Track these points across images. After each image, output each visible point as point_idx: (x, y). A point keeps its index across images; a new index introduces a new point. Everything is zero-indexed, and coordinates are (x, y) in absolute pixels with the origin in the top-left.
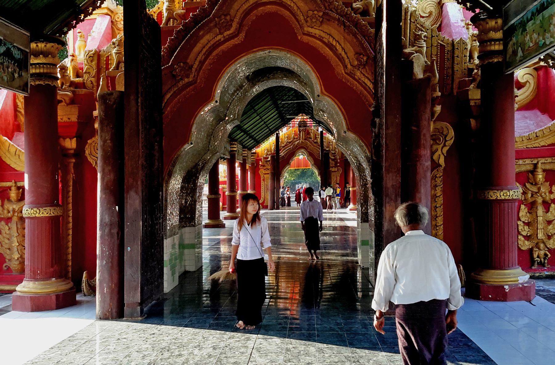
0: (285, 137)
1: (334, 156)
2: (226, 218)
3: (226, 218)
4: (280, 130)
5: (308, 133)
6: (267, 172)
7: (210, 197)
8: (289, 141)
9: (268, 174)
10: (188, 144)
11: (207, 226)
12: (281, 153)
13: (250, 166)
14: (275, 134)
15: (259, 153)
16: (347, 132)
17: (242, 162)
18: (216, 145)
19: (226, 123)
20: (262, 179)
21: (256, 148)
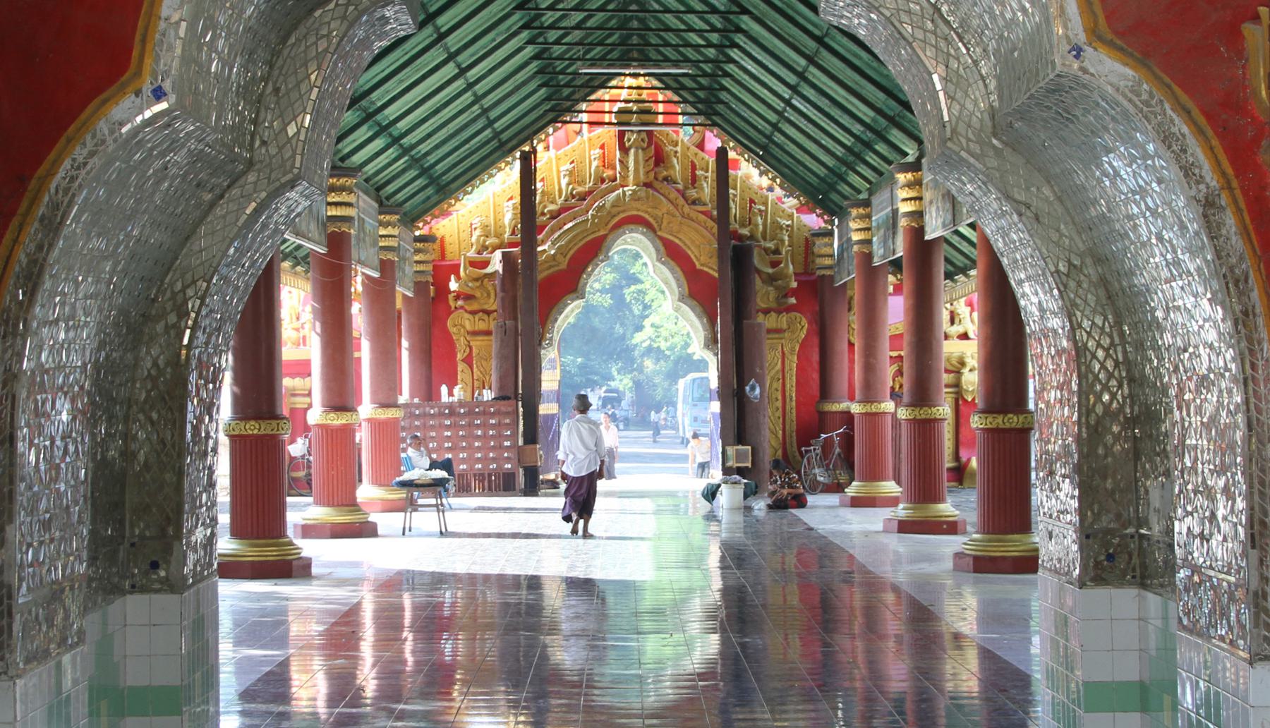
0: (559, 172)
1: (775, 264)
2: (309, 531)
3: (309, 531)
6: (482, 326)
8: (580, 189)
9: (488, 333)
11: (232, 569)
12: (543, 242)
13: (410, 294)
14: (518, 154)
15: (447, 240)
17: (376, 275)
18: (289, 140)
19: (344, 18)
20: (459, 356)
21: (435, 217)
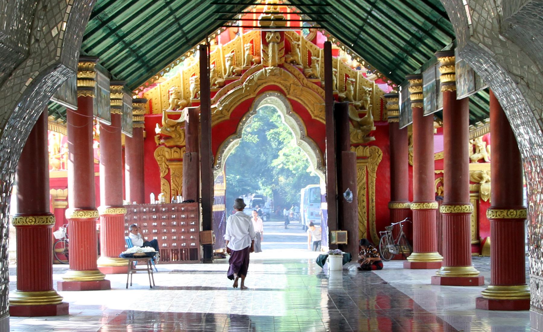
0: (224, 58)
1: (361, 116)
2: (67, 286)
3: (67, 286)
5: (288, 49)
6: (176, 156)
7: (21, 224)
8: (238, 69)
14: (198, 47)
15: (154, 101)
17: (108, 124)
18: (53, 39)
20: (162, 175)
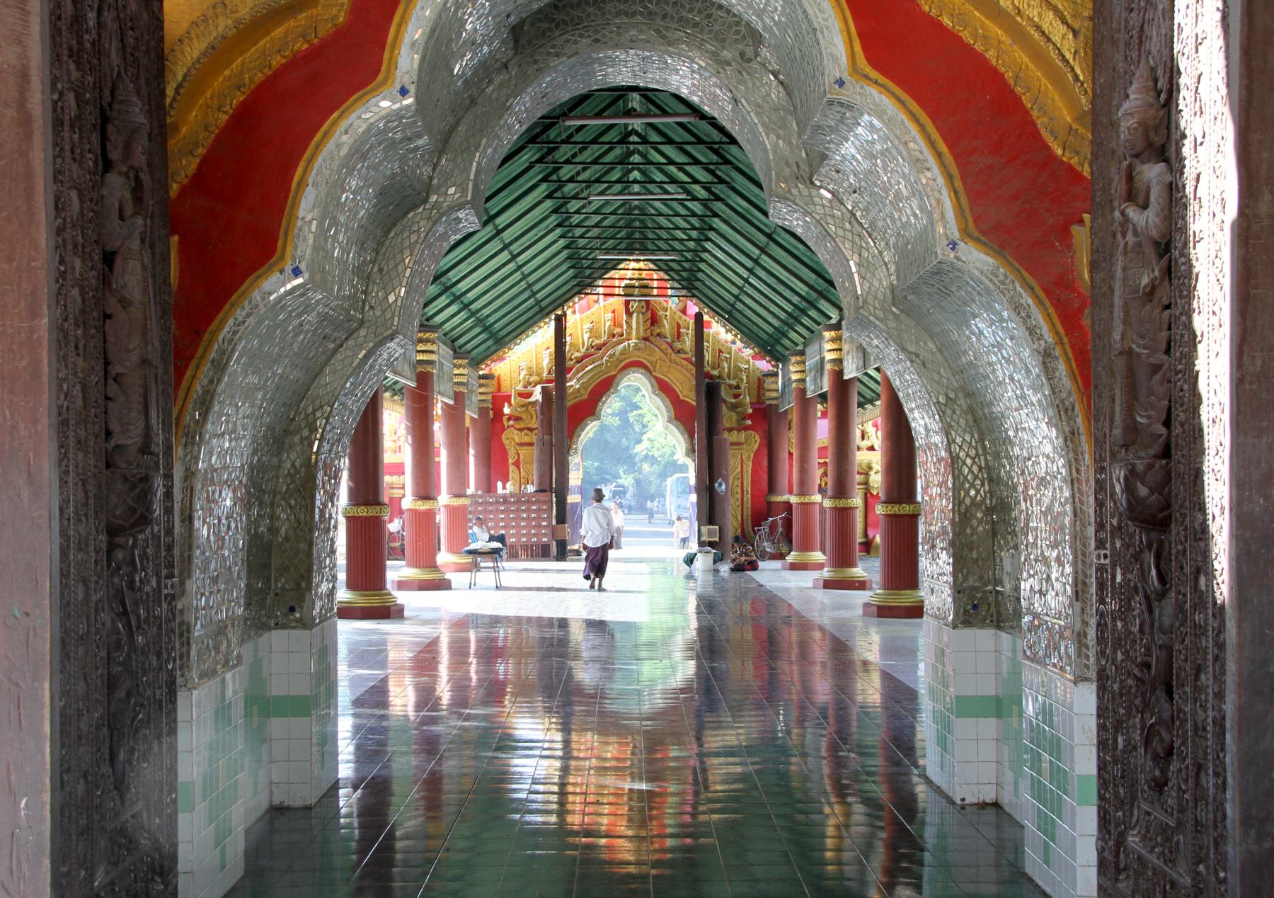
0: (582, 330)
1: (736, 396)
4: (569, 307)
5: (654, 320)
6: (527, 439)
7: (351, 515)
8: (597, 342)
9: (531, 444)
10: (282, 272)
12: (571, 379)
13: (476, 416)
14: (553, 317)
15: (502, 378)
16: (961, 244)
17: (451, 402)
18: (390, 306)
19: (429, 218)
20: (511, 461)
